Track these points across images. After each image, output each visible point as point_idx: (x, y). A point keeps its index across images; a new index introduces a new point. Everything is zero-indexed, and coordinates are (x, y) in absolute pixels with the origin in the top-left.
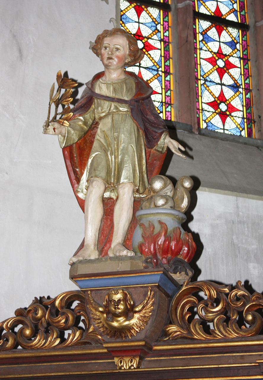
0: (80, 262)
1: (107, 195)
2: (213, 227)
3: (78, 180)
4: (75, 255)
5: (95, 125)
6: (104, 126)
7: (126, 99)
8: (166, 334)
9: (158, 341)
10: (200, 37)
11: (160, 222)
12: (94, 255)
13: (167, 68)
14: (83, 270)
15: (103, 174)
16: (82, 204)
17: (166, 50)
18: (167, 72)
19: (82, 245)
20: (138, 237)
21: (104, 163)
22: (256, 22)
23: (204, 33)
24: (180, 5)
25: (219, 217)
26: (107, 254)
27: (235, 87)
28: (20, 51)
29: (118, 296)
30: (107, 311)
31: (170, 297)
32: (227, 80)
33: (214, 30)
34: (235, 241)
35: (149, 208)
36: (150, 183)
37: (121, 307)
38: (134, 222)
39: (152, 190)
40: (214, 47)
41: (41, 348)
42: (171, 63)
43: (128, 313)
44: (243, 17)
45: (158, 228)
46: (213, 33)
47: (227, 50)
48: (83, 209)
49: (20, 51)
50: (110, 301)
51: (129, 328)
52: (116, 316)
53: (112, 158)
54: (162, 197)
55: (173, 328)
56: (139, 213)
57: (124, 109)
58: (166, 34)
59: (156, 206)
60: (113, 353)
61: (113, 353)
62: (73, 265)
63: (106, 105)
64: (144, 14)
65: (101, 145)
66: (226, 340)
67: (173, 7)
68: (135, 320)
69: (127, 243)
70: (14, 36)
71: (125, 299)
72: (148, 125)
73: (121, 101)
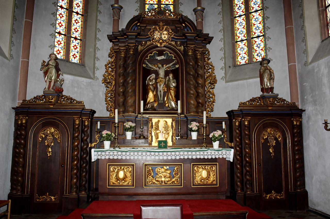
0: (45, 91)
1: (50, 80)
2: (69, 81)
3: (45, 77)
4: (44, 89)
5: (49, 68)
6: (50, 69)
7: (54, 65)
8: (58, 102)
9: (56, 103)
10: (71, 42)
11: (58, 86)
12: (47, 90)
13: (64, 48)
14: (45, 92)
15: (49, 78)
16: (46, 81)
17: (64, 44)
18: (64, 49)
19: (45, 88)
20: (54, 88)
21: (50, 76)
22: (83, 39)
23: (73, 41)
24: (68, 35)
25: (70, 80)
26: (49, 90)
27: (78, 52)
28: (35, 47)
29: (51, 97)
30: (49, 99)
31: (59, 97)
32: (76, 51)
33: (75, 40)
34: (73, 84)
35: (56, 83)
36: (57, 79)
37: (51, 98)
38: (54, 85)
39: (57, 80)
40: (74, 44)
41: (38, 103)
42: (65, 47)
43: (52, 99)
44: (81, 38)
45: (57, 87)
46: (74, 41)
47: (77, 45)
48: (46, 82)
49: (35, 47)
50: (49, 97)
51: (52, 101)
52: (50, 100)
53: (51, 75)
54: (59, 82)
55: (59, 102)
56: (55, 84)
57: (53, 67)
58: (65, 41)
59: (58, 83)
60: (49, 105)
61: (49, 105)
62: (44, 91)
63: (51, 66)
64: (60, 36)
65: (50, 73)
66: (66, 104)
67: (66, 35)
68: (53, 100)
69: (53, 88)
70: (34, 44)
71: (52, 97)
72: (57, 70)
73: (53, 66)
